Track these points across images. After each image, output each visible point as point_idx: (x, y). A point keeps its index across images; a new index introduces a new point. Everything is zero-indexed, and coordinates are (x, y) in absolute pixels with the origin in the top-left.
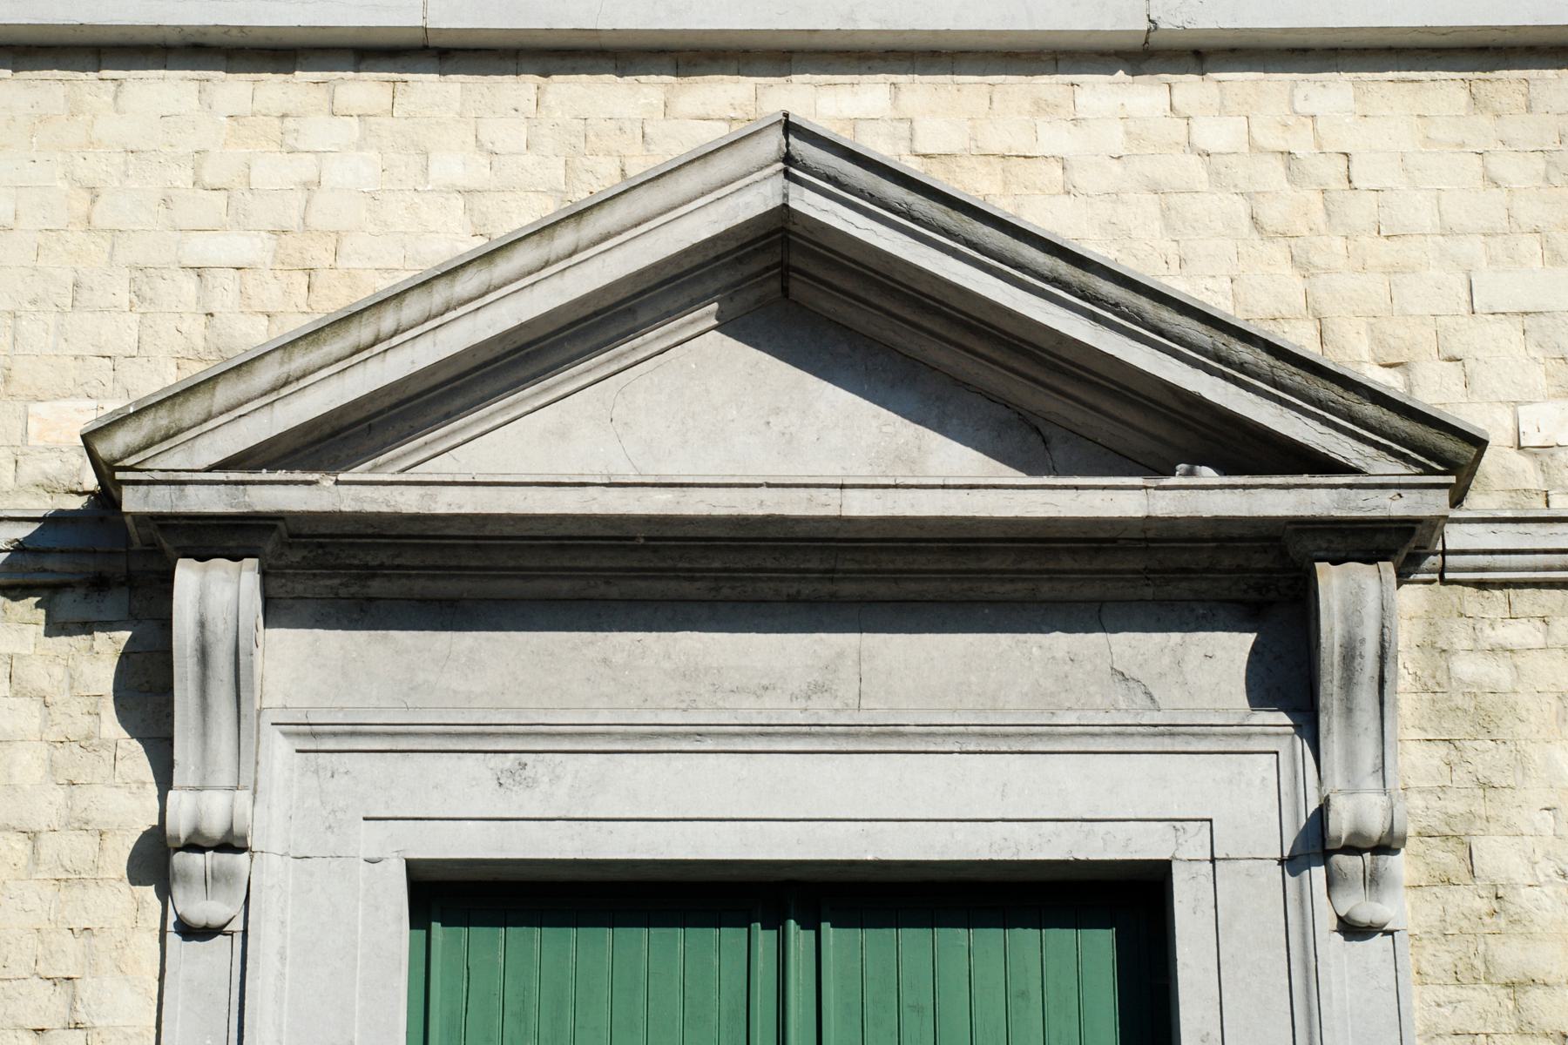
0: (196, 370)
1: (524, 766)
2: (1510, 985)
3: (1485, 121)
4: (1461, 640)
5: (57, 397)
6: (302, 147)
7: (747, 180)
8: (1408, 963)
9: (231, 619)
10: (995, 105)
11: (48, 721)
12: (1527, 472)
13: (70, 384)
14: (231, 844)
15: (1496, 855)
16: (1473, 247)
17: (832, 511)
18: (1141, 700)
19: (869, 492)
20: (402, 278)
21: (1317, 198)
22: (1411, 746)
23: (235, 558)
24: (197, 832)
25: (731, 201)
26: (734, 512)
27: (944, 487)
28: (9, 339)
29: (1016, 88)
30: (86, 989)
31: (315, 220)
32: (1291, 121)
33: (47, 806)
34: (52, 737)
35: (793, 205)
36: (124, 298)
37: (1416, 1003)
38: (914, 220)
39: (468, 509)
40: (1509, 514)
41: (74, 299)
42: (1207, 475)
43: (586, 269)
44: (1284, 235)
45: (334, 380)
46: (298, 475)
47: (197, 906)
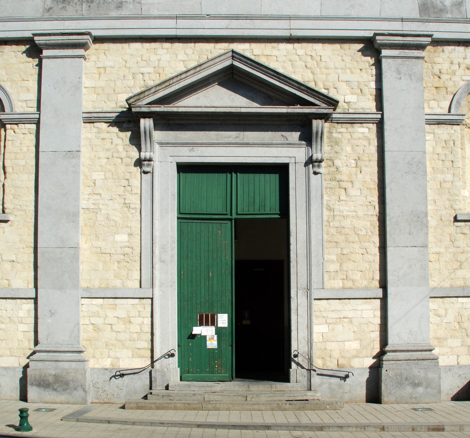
0: (143, 89)
1: (193, 148)
2: (338, 181)
3: (342, 51)
4: (334, 131)
5: (122, 93)
6: (157, 54)
7: (227, 60)
8: (323, 178)
9: (149, 127)
10: (266, 47)
11: (123, 142)
12: (346, 106)
13: (124, 91)
14: (150, 160)
15: (338, 163)
16: (339, 71)
17: (239, 111)
18: (286, 139)
19: (245, 108)
20: (174, 74)
21: (315, 63)
22: (326, 147)
23: (149, 118)
24: (145, 158)
25: (224, 63)
26: (224, 111)
27: (256, 108)
28: (114, 84)
29: (269, 46)
30: (130, 180)
31: (160, 65)
32: (312, 50)
33: (123, 154)
34: (124, 144)
35: (234, 64)
36: (131, 78)
37: (324, 183)
38: (252, 66)
39: (184, 111)
40: (342, 112)
41: (124, 78)
42: (299, 106)
43: (202, 74)
44: (310, 68)
45: (163, 91)
46: (158, 106)
47: (146, 169)
